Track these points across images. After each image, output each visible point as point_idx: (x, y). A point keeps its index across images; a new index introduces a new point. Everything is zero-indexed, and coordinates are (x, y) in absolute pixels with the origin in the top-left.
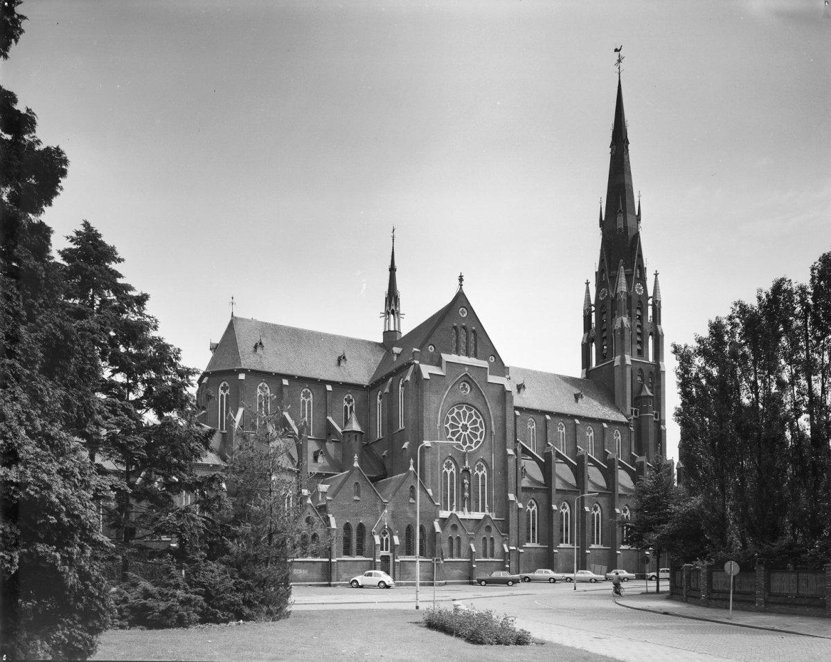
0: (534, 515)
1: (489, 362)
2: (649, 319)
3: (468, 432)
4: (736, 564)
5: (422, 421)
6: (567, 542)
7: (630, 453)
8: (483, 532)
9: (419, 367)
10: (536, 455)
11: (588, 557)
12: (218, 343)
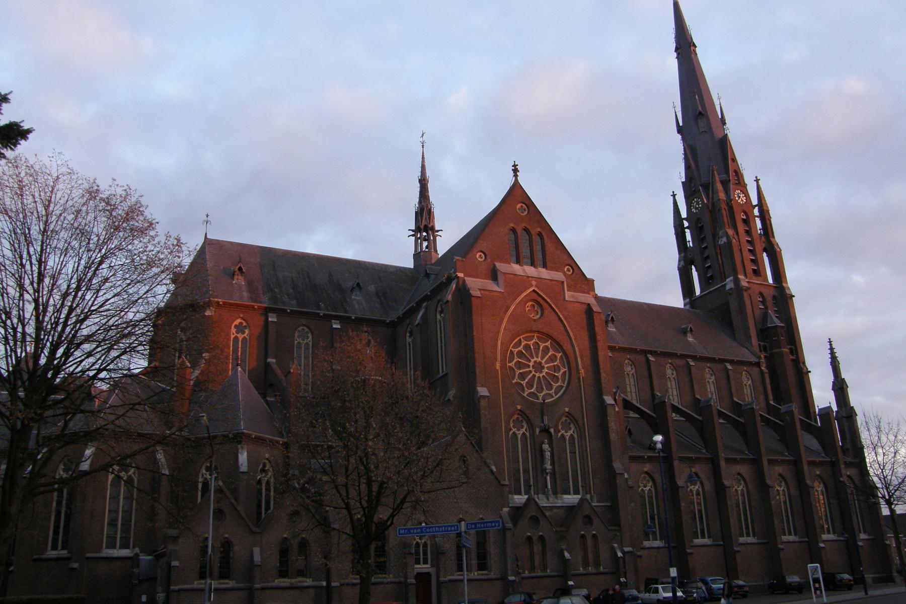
1: (565, 274)
2: (759, 232)
4: (524, 501)
5: (474, 358)
6: (703, 537)
9: (464, 281)
10: (640, 407)
11: (738, 556)
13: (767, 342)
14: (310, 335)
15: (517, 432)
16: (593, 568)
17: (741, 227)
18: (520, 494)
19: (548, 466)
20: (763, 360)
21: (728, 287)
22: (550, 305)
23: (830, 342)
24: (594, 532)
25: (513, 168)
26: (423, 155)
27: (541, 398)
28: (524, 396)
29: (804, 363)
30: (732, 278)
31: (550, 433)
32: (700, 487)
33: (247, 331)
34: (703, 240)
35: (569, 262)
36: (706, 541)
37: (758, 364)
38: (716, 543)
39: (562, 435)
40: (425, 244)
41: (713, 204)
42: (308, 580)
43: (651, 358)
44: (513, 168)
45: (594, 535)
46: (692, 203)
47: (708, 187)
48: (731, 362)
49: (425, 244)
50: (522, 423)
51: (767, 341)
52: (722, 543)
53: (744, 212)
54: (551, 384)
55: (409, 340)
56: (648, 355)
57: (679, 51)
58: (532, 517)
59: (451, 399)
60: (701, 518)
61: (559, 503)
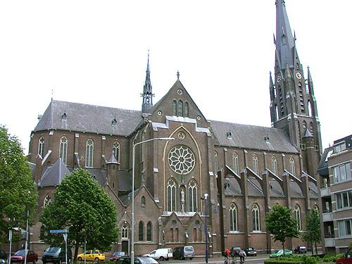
0: (235, 213)
6: (258, 230)
19: (183, 200)
36: (259, 232)
37: (298, 154)
40: (147, 100)
43: (246, 151)
48: (285, 153)
58: (173, 221)
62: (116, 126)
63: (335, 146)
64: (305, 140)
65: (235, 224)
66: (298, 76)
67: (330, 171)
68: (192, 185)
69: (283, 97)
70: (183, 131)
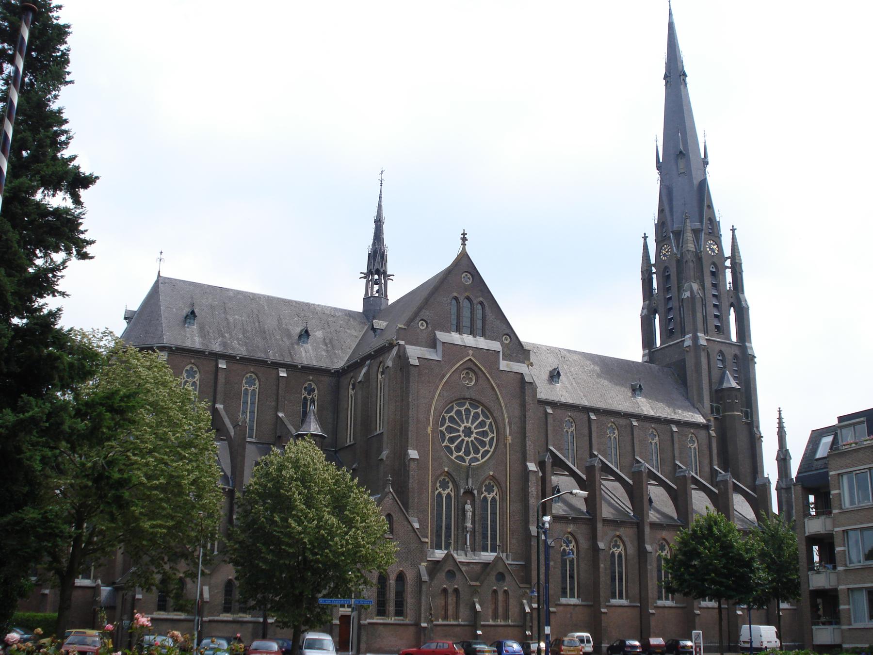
2: (728, 286)
3: (472, 438)
6: (621, 597)
7: (712, 468)
8: (491, 584)
9: (405, 349)
12: (136, 310)
13: (721, 404)
14: (257, 382)
15: (442, 492)
16: (502, 620)
17: (708, 280)
18: (441, 548)
19: (469, 525)
20: (712, 423)
21: (686, 344)
22: (484, 374)
23: (780, 411)
24: (506, 588)
25: (462, 236)
26: (381, 194)
27: (467, 461)
28: (451, 459)
29: (758, 427)
30: (690, 335)
31: (474, 494)
32: (623, 550)
33: (197, 376)
34: (668, 290)
35: (507, 331)
36: (624, 602)
38: (632, 604)
39: (485, 497)
40: (376, 287)
41: (682, 254)
42: (248, 616)
44: (462, 236)
45: (505, 591)
46: (661, 249)
47: (679, 234)
49: (376, 287)
50: (448, 483)
51: (721, 402)
52: (639, 605)
53: (714, 264)
54: (478, 448)
55: (351, 392)
56: (590, 414)
57: (668, 79)
58: (449, 571)
59: (385, 459)
60: (621, 579)
61: (476, 559)
62: (308, 346)
63: (841, 428)
64: (720, 395)
65: (572, 583)
66: (709, 247)
67: (833, 483)
68: (490, 490)
69: (673, 294)
70: (471, 368)
